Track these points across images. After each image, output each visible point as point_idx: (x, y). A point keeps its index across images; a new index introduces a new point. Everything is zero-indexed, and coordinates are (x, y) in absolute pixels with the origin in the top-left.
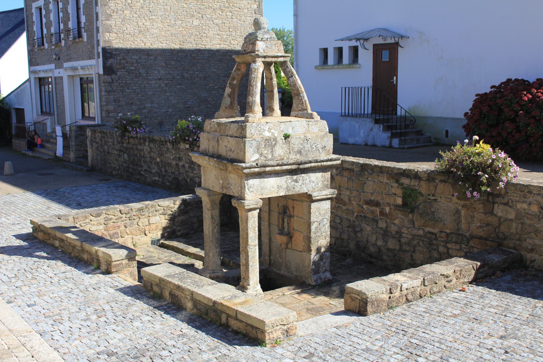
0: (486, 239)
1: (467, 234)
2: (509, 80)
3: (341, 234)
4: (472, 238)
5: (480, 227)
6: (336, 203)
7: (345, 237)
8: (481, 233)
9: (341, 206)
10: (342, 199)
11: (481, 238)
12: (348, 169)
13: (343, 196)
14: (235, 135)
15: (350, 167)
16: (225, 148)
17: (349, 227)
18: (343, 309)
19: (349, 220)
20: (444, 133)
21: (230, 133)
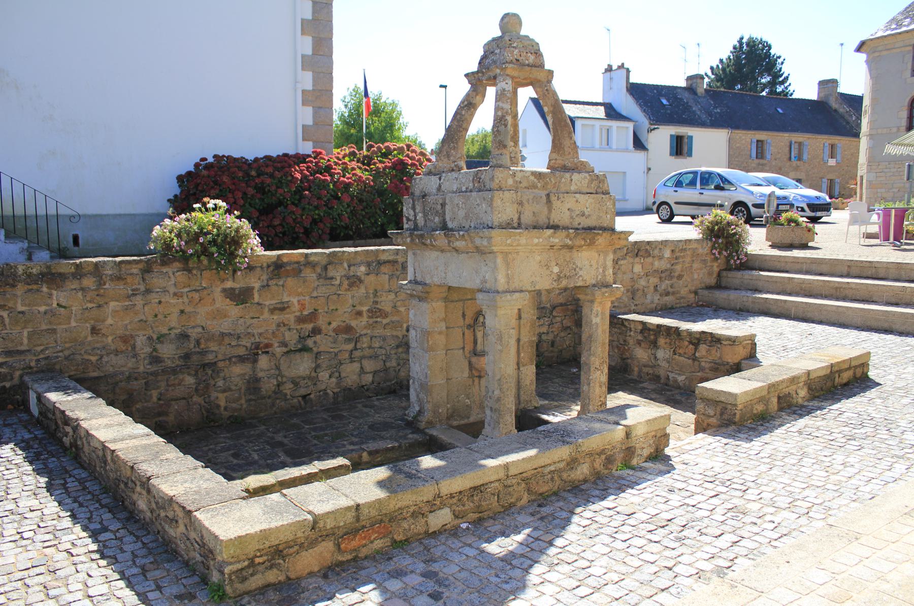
0: (565, 304)
1: (548, 306)
2: (243, 158)
3: (384, 362)
4: (554, 308)
5: (560, 294)
6: (369, 317)
7: (392, 363)
8: (561, 300)
9: (379, 319)
10: (380, 310)
11: (561, 305)
12: (389, 262)
13: (383, 304)
14: (585, 190)
15: (391, 258)
16: (568, 213)
17: (398, 347)
18: (627, 410)
19: (397, 336)
20: (71, 240)
21: (573, 188)
